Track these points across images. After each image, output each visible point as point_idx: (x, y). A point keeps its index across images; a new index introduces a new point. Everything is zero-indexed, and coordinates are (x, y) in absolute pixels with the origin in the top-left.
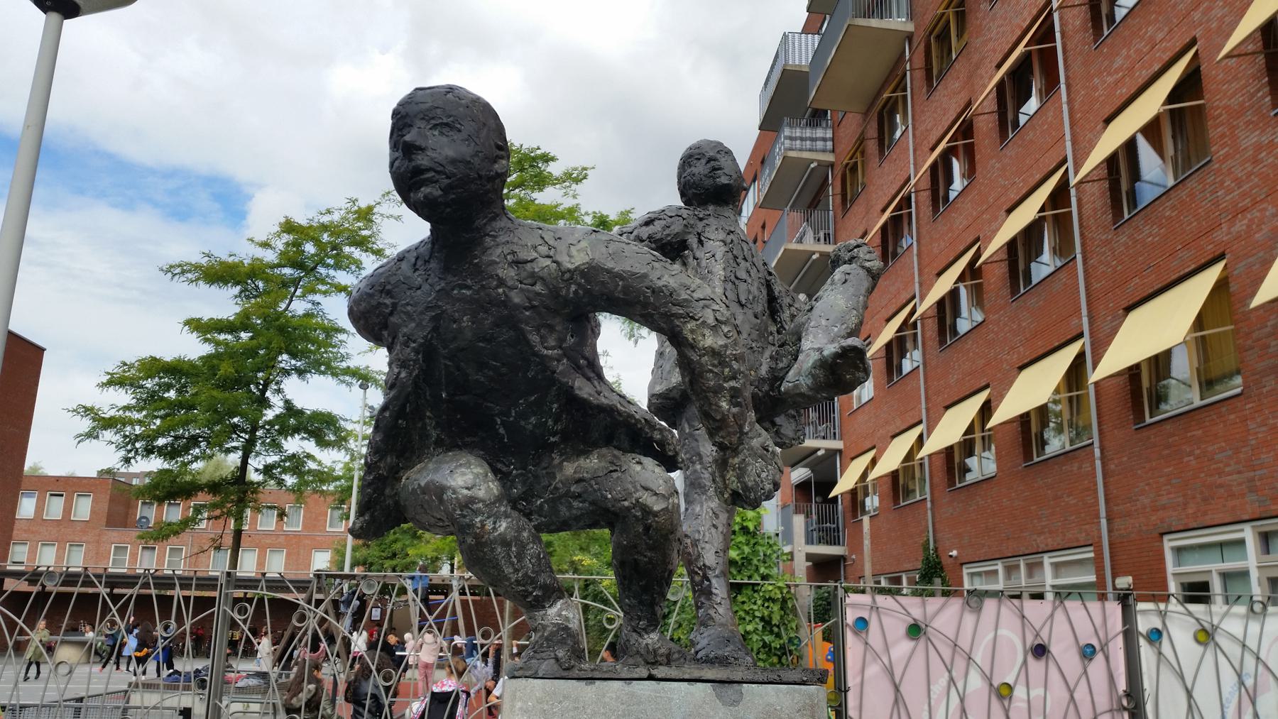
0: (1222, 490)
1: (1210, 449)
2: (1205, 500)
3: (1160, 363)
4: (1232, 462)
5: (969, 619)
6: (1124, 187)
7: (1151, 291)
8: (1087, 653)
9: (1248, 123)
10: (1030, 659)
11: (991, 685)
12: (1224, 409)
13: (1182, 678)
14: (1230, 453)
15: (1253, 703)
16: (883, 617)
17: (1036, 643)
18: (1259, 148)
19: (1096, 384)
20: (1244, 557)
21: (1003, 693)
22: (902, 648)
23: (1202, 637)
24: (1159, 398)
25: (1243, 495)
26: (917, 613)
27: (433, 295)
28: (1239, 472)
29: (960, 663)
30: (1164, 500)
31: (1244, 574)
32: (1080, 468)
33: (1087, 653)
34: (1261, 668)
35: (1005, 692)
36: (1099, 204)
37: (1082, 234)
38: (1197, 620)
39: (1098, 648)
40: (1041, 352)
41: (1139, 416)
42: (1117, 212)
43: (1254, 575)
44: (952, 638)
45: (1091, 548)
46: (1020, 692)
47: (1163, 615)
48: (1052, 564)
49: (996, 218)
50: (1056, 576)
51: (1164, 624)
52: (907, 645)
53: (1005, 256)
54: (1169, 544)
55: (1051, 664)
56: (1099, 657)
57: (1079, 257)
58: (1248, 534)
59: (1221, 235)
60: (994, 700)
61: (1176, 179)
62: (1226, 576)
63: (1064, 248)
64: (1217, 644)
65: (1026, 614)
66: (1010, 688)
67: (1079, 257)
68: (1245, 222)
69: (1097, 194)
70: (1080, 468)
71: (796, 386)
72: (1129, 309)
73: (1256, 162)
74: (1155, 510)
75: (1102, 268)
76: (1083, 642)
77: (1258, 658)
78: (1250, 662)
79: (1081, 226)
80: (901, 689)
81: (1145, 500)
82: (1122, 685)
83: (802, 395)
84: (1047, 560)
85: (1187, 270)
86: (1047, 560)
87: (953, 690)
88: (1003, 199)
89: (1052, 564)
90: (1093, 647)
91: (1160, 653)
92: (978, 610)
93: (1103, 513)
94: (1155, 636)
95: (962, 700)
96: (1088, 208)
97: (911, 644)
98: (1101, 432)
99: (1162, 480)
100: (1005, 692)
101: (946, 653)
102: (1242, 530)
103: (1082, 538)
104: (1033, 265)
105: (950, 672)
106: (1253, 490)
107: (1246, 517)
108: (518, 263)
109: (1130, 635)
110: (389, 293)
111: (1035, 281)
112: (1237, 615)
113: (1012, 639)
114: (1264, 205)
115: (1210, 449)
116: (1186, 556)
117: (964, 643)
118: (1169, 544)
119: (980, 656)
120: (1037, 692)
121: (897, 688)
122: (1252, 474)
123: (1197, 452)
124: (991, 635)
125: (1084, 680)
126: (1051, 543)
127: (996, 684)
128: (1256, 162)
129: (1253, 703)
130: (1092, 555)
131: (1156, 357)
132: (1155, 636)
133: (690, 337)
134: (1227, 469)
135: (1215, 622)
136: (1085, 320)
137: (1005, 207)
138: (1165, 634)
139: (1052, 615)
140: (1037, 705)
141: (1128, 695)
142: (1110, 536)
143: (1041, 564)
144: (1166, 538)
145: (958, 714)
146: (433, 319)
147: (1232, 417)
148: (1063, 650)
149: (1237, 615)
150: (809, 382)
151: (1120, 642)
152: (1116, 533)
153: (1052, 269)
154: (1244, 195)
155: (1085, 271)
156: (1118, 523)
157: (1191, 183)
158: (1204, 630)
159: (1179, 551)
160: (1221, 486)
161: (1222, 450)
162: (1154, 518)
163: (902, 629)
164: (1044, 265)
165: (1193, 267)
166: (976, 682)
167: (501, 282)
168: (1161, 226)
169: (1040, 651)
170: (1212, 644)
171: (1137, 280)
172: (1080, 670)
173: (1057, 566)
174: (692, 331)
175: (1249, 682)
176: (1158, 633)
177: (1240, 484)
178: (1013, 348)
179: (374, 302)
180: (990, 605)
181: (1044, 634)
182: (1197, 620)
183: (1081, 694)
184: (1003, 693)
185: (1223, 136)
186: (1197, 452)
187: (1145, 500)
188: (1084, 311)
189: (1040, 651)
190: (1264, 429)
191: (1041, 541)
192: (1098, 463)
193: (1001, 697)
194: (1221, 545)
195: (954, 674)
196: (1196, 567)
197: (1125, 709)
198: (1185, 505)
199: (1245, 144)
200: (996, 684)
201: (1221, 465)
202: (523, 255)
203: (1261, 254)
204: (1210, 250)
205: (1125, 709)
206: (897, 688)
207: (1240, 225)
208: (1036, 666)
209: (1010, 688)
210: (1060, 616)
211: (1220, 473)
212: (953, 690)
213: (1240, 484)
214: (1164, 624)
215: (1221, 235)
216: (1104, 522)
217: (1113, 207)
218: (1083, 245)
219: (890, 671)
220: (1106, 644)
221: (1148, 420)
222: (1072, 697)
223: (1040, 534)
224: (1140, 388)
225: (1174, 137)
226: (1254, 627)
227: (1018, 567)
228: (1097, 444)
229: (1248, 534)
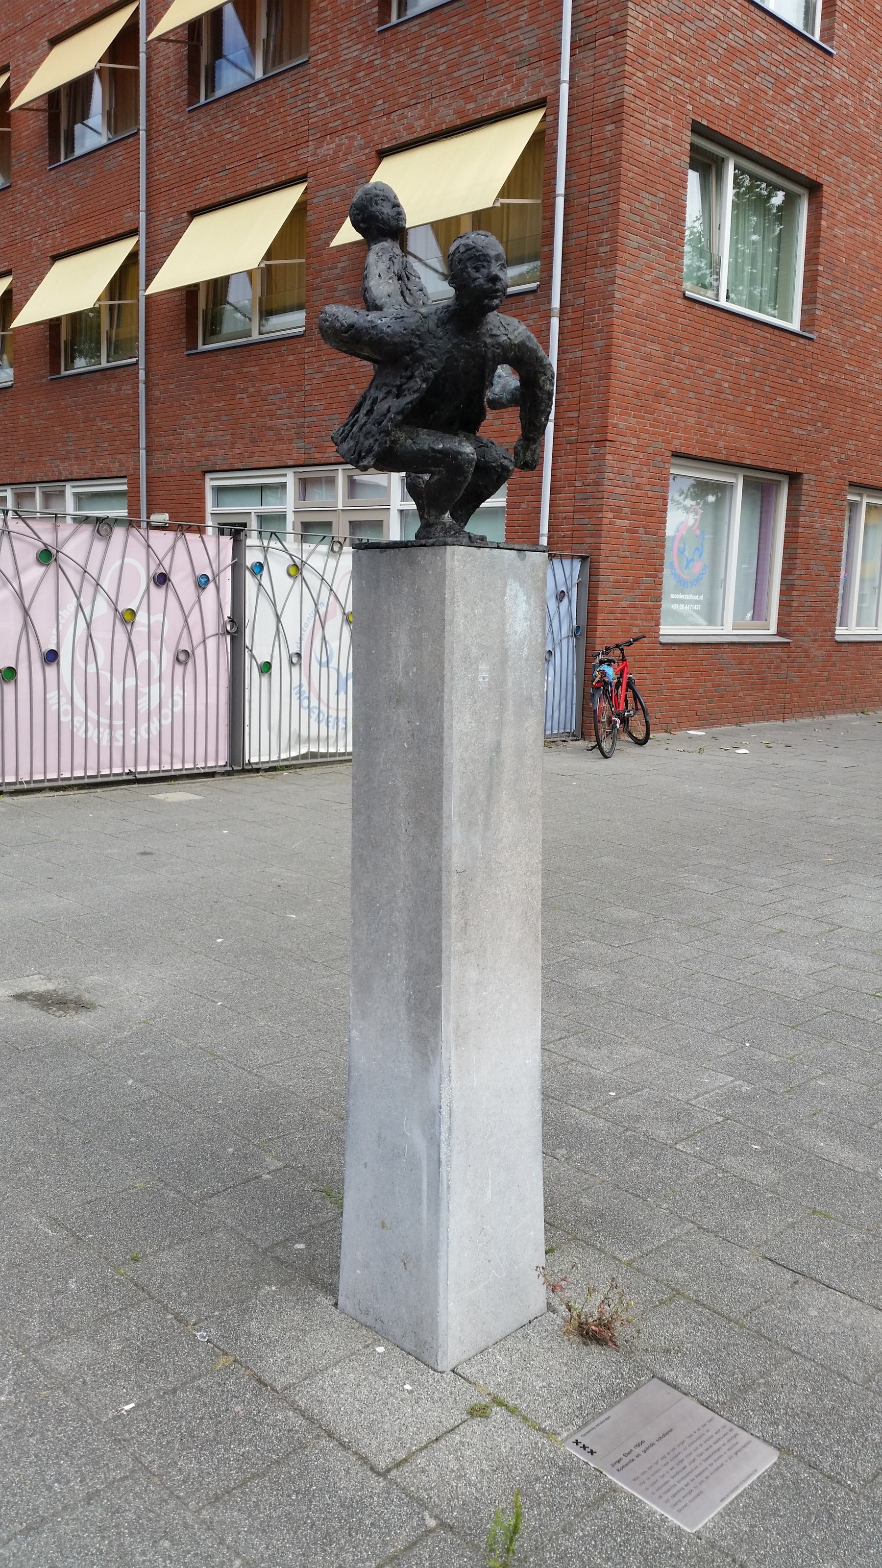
0: (271, 433)
1: (265, 388)
2: (253, 441)
3: (219, 287)
4: (284, 406)
5: (99, 546)
6: (204, 60)
7: (222, 198)
8: (202, 583)
9: (352, 31)
10: (152, 586)
11: (116, 610)
12: (283, 348)
13: (274, 605)
14: (284, 395)
15: (323, 628)
16: (15, 542)
17: (159, 572)
18: (358, 65)
19: (148, 298)
20: (283, 502)
21: (127, 618)
22: (33, 573)
23: (292, 572)
24: (213, 327)
25: (291, 440)
26: (48, 538)
27: (450, 345)
28: (290, 417)
29: (88, 590)
30: (211, 436)
31: (282, 517)
32: (119, 390)
33: (202, 583)
34: (332, 597)
35: (128, 617)
36: (173, 72)
37: (148, 105)
38: (291, 555)
39: (211, 578)
40: (83, 242)
41: (192, 342)
42: (194, 94)
43: (290, 518)
44: (83, 565)
45: (125, 481)
46: (141, 618)
47: (265, 550)
48: (75, 494)
49: (34, 48)
50: (78, 507)
51: (266, 558)
52: (39, 570)
53: (46, 106)
54: (210, 482)
55: (170, 593)
56: (211, 587)
57: (143, 134)
58: (290, 479)
59: (307, 154)
60: (118, 623)
61: (264, 74)
62: (262, 518)
63: (120, 114)
64: (303, 579)
65: (151, 544)
66: (133, 613)
67: (143, 134)
68: (333, 146)
69: (172, 60)
70: (119, 390)
71: (500, 398)
72: (195, 214)
73: (354, 81)
74: (201, 446)
75: (169, 156)
76: (199, 573)
77: (331, 590)
78: (325, 591)
79: (148, 95)
80: (31, 613)
81: (190, 434)
82: (227, 612)
83: (502, 403)
84: (70, 490)
85: (265, 185)
86: (70, 490)
87: (80, 614)
88: (46, 22)
89: (75, 494)
90: (207, 577)
91: (260, 584)
92: (108, 538)
93: (143, 443)
94: (259, 568)
95: (89, 626)
96: (159, 75)
97: (41, 570)
98: (147, 351)
99: (211, 415)
100: (128, 617)
101: (75, 580)
102: (285, 475)
103: (115, 468)
104: (78, 128)
105: (78, 598)
106: (301, 436)
107: (291, 463)
108: (492, 336)
109: (237, 568)
110: (419, 337)
111: (78, 152)
112: (320, 553)
113: (138, 570)
114: (355, 133)
115: (265, 388)
116: (227, 497)
117: (93, 569)
118: (210, 482)
119: (108, 582)
120: (156, 618)
121: (26, 612)
122: (302, 420)
123: (251, 390)
124: (119, 563)
125: (197, 607)
126: (76, 471)
127: (121, 609)
128: (354, 81)
129: (323, 628)
130: (125, 488)
131: (216, 281)
132: (259, 568)
133: (542, 384)
134: (279, 412)
135: (304, 559)
136: (142, 215)
137: (48, 35)
138: (265, 568)
139: (173, 547)
140: (156, 630)
141: (232, 621)
142: (147, 470)
143: (62, 493)
144: (208, 476)
145: (85, 639)
146: (448, 358)
147: (291, 358)
148: (182, 580)
149: (320, 553)
150: (509, 397)
151: (229, 573)
152: (155, 466)
153: (103, 140)
154: (336, 115)
155: (148, 154)
156: (158, 456)
157: (284, 83)
158: (295, 565)
159: (219, 490)
160: (271, 429)
161: (277, 392)
162: (198, 454)
163: (32, 556)
164: (92, 134)
165: (272, 182)
166: (102, 609)
167: (486, 345)
168: (243, 124)
169: (162, 579)
170: (300, 577)
171: (207, 182)
172: (194, 598)
173: (78, 497)
174: (543, 381)
175: (322, 610)
176: (261, 566)
177: (289, 429)
178: (46, 231)
179: (406, 339)
180: (119, 533)
181: (166, 563)
182: (291, 555)
183: (194, 619)
184: (127, 618)
185: (324, 36)
186: (251, 390)
187: (190, 434)
188: (143, 206)
189: (162, 579)
190: (320, 375)
191: (65, 469)
192: (142, 387)
193: (124, 622)
194: (262, 488)
195: (82, 600)
196: (234, 507)
197: (228, 633)
198: (233, 445)
199: (346, 55)
200: (121, 609)
201: (274, 407)
202: (495, 332)
203: (343, 187)
204: (292, 169)
205: (228, 633)
206: (26, 612)
207: (327, 148)
208: (157, 594)
209: (133, 613)
210: (180, 545)
211: (272, 416)
212: (80, 614)
213: (289, 429)
214: (266, 558)
215: (307, 154)
216: (143, 453)
217: (190, 83)
218: (148, 119)
219: (20, 596)
220: (218, 575)
221: (201, 348)
222: (186, 621)
223: (63, 460)
224: (196, 308)
225: (269, 15)
226: (332, 562)
227: (33, 495)
228: (142, 365)
229: (290, 479)
